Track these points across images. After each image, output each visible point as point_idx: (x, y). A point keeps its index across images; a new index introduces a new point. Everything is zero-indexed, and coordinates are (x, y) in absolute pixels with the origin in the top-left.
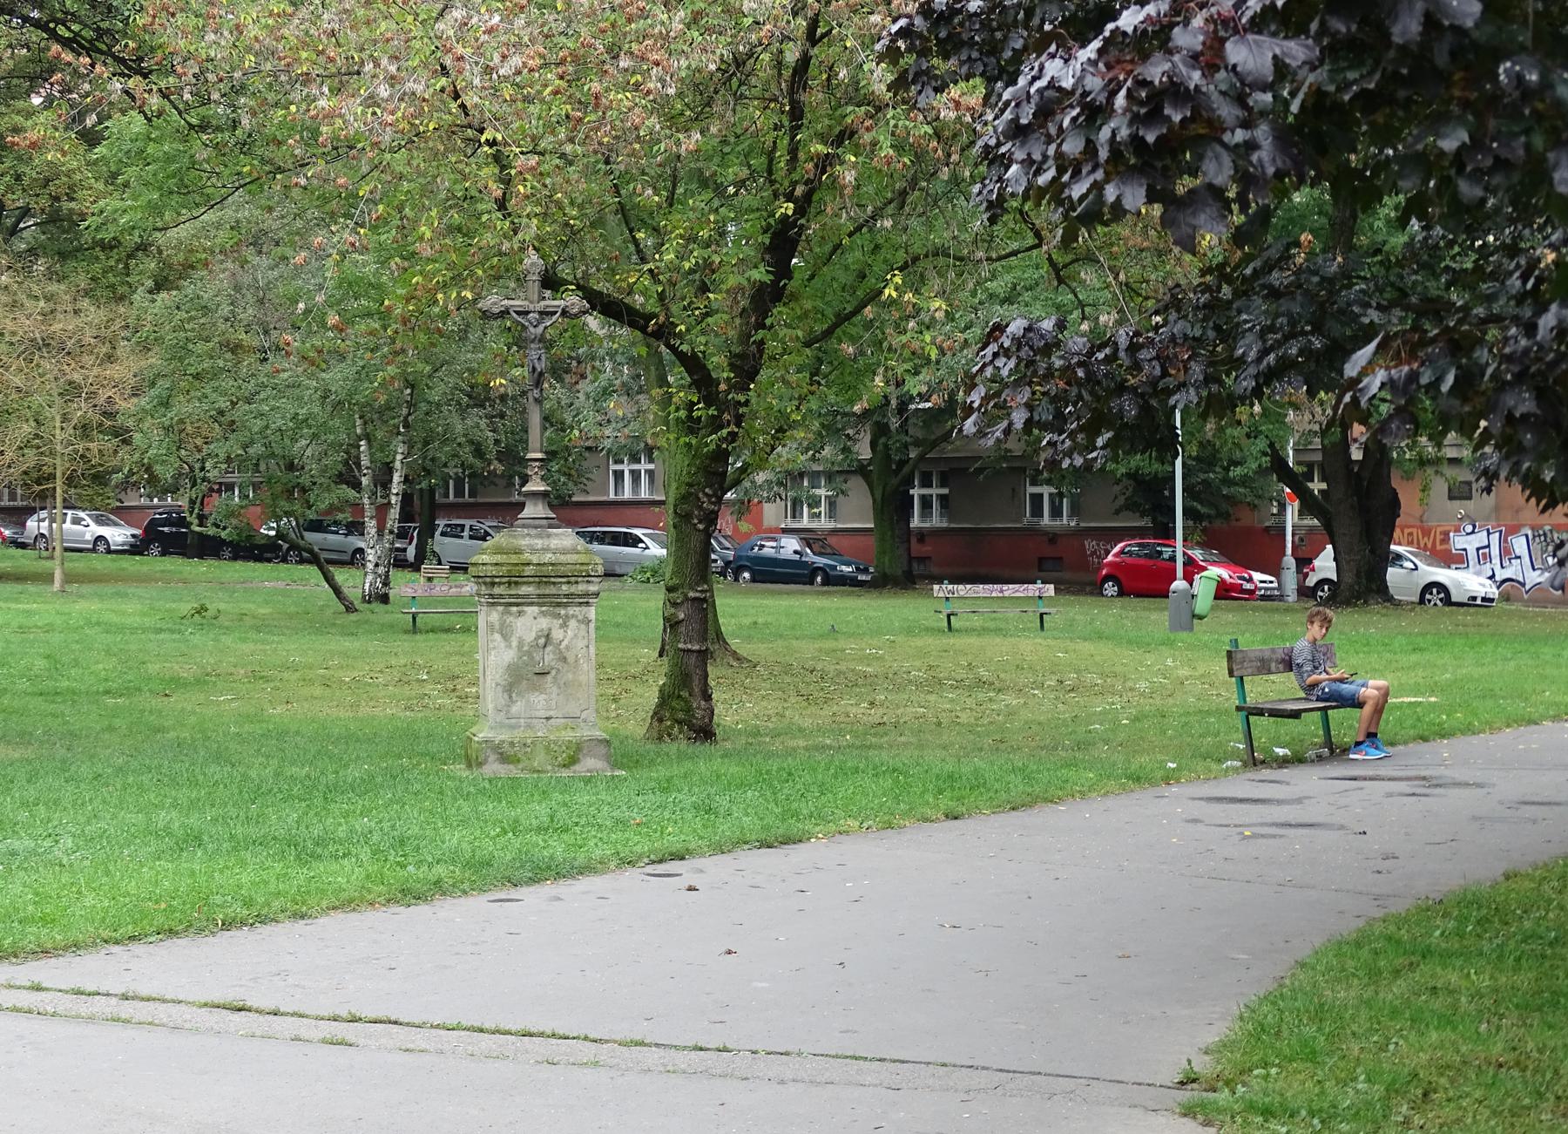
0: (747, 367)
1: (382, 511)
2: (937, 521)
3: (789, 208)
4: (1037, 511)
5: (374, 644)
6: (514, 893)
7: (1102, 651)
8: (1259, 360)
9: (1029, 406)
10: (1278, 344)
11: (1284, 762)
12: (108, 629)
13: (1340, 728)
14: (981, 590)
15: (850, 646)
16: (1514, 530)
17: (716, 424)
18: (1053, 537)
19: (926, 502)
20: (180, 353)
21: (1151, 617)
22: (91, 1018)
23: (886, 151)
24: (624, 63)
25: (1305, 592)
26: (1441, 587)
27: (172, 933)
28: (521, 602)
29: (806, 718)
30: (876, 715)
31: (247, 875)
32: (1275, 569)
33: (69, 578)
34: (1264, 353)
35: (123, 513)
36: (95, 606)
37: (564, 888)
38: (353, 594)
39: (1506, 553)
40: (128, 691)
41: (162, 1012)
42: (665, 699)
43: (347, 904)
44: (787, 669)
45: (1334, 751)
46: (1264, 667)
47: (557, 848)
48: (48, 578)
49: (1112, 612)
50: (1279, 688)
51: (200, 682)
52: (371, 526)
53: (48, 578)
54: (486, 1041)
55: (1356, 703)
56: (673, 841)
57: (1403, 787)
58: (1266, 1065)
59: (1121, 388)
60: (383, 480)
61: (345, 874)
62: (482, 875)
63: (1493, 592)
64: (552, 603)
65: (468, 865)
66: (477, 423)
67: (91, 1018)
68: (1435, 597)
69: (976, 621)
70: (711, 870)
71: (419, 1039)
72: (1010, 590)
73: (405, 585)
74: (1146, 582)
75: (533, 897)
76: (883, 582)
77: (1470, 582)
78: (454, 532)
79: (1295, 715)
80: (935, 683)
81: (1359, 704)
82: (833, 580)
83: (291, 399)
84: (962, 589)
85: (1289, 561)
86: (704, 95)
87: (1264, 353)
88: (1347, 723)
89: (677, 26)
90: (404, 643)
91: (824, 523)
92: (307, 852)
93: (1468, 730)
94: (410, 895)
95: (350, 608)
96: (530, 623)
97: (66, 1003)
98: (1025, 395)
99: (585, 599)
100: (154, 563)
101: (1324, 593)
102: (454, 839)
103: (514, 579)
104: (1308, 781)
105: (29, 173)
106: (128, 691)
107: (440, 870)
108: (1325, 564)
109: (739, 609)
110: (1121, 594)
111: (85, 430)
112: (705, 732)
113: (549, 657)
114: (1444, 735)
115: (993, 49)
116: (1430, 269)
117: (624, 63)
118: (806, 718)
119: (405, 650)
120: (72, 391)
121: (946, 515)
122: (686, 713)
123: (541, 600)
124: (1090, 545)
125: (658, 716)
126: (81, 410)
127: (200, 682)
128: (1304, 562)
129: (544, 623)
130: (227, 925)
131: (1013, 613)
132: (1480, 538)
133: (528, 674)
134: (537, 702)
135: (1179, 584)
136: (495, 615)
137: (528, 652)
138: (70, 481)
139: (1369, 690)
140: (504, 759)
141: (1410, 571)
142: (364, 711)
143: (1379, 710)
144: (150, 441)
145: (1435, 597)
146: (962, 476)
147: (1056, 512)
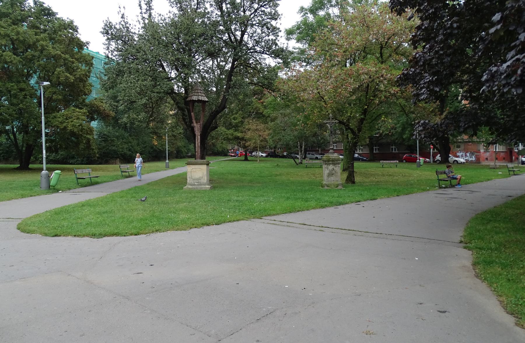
0: (360, 130)
1: (301, 152)
2: (377, 152)
3: (366, 107)
4: (392, 150)
5: (302, 170)
6: (338, 207)
7: (408, 170)
8: (464, 126)
9: (424, 134)
10: (468, 124)
11: (445, 188)
12: (266, 167)
13: (453, 183)
14: (387, 162)
15: (369, 170)
16: (467, 152)
17: (355, 138)
18: (395, 154)
19: (376, 149)
20: (274, 131)
21: (414, 166)
22: (284, 226)
23: (383, 98)
24: (344, 87)
25: (434, 161)
26: (456, 161)
27: (291, 212)
28: (330, 164)
29: (367, 180)
30: (377, 180)
31: (298, 204)
32: (429, 158)
33: (260, 161)
34: (465, 125)
35: (265, 152)
36: (263, 164)
37: (344, 206)
38: (297, 162)
39: (466, 156)
40: (271, 176)
41: (294, 225)
42: (348, 177)
43: (314, 208)
44: (361, 173)
45: (452, 186)
46: (441, 173)
47: (341, 200)
48: (257, 161)
49: (405, 165)
50: (443, 176)
51: (280, 175)
52: (300, 153)
53: (257, 161)
54: (344, 231)
55: (456, 179)
56: (357, 199)
57: (467, 192)
58: (474, 240)
59: (439, 131)
60: (301, 147)
61: (313, 203)
62: (332, 204)
63: (465, 161)
64: (334, 164)
65: (330, 202)
66: (314, 139)
67: (284, 226)
68: (455, 162)
69: (386, 166)
70: (365, 203)
71: (333, 230)
72: (392, 161)
73: (304, 161)
74: (413, 160)
75: (340, 207)
76: (371, 160)
77: (462, 160)
78: (309, 154)
79: (447, 181)
80: (383, 175)
81: (457, 179)
82: (363, 160)
83: (289, 136)
84: (384, 161)
85: (431, 157)
86: (354, 92)
87: (465, 125)
88: (454, 182)
89: (352, 81)
90: (306, 169)
91: (361, 152)
92: (307, 200)
93: (472, 183)
94: (322, 207)
95: (297, 165)
96: (331, 167)
97: (280, 223)
98: (424, 132)
99: (339, 164)
100: (269, 159)
101: (438, 162)
102: (327, 198)
103: (329, 161)
104: (450, 191)
105: (254, 107)
106: (271, 176)
107: (326, 203)
108: (438, 157)
109: (356, 164)
110: (406, 162)
111: (261, 141)
112: (354, 182)
113: (334, 172)
114: (469, 184)
115: (414, 79)
116: (82, 131)
117: (344, 87)
118: (367, 180)
119: (306, 170)
120: (260, 136)
121: (384, 150)
122: (351, 180)
123: (333, 164)
124: (400, 155)
125: (346, 180)
126: (261, 138)
127: (280, 175)
128: (434, 157)
129: (333, 167)
130: (298, 211)
131: (392, 165)
132: (462, 153)
133: (331, 174)
134: (332, 178)
135: (418, 161)
136: (326, 166)
137: (331, 171)
138: (260, 148)
139: (459, 176)
140: (328, 186)
141: (452, 158)
142: (303, 179)
143: (460, 180)
144: (271, 142)
145: (455, 162)
146: (381, 145)
147: (395, 150)
